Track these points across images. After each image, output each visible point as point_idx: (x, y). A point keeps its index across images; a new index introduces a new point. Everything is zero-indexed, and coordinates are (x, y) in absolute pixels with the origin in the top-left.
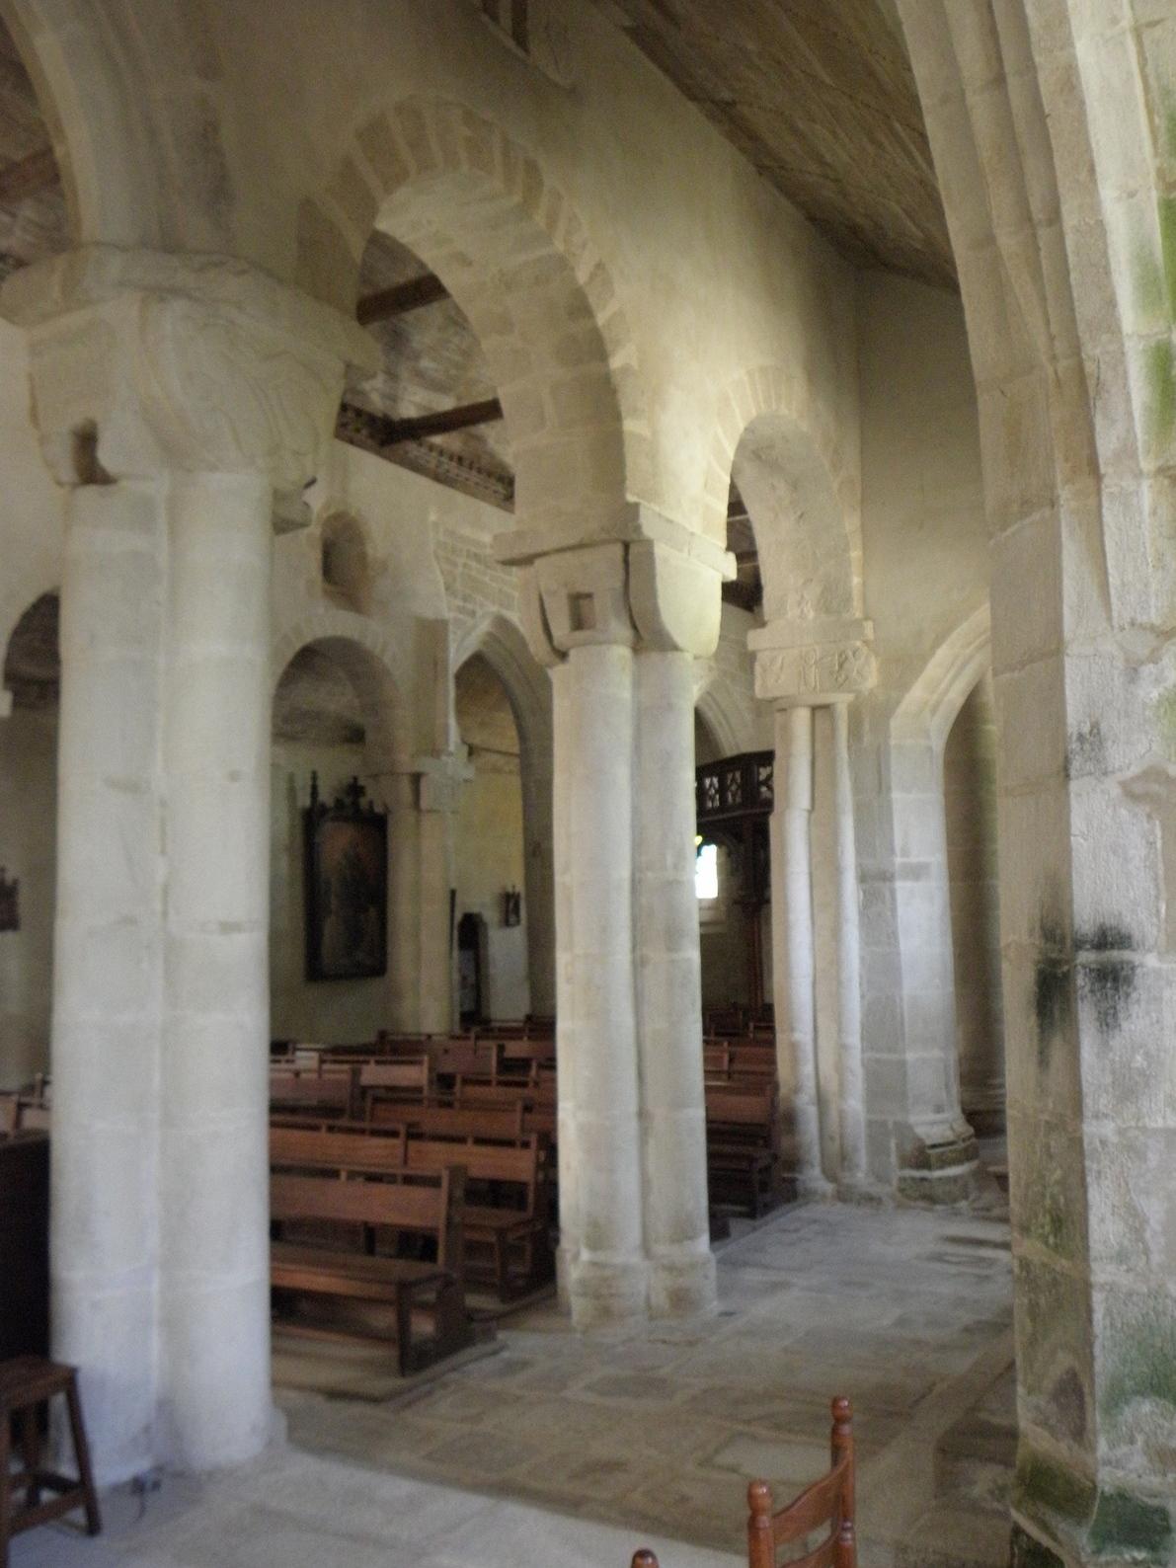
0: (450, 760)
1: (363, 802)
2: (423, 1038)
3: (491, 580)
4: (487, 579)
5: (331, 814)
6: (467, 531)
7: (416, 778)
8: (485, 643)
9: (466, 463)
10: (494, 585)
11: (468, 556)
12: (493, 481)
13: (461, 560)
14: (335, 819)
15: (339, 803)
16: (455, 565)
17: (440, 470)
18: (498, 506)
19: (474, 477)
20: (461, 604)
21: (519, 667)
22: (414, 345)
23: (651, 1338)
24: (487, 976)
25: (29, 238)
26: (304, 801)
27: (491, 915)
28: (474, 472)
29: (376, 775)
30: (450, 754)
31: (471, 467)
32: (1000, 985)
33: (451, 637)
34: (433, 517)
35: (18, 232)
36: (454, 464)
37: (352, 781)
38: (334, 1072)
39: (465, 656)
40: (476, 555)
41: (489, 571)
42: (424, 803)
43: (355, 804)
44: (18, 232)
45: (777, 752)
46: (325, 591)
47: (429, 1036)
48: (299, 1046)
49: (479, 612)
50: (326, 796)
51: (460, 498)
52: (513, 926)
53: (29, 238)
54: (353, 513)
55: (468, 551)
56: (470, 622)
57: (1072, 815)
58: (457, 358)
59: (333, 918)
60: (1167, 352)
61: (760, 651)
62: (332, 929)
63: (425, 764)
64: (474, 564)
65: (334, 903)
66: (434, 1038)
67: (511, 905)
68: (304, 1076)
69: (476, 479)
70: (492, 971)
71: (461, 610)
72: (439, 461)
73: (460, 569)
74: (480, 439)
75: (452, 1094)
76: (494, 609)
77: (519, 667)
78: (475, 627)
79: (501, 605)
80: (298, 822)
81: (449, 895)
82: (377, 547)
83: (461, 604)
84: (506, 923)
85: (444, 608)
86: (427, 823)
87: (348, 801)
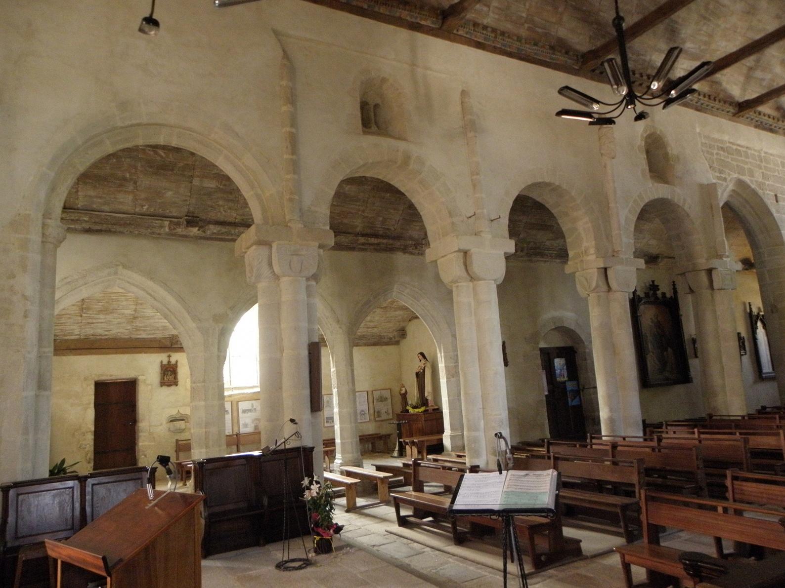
3: (732, 160)
4: (730, 160)
6: (716, 136)
7: (710, 272)
9: (712, 98)
10: (733, 162)
11: (718, 149)
12: (727, 105)
13: (715, 151)
14: (645, 303)
15: (647, 295)
16: (712, 154)
18: (730, 120)
19: (717, 105)
20: (719, 175)
21: (752, 207)
22: (683, 36)
23: (204, 398)
25: (497, 17)
28: (717, 102)
29: (684, 273)
31: (715, 100)
35: (491, 14)
36: (706, 99)
37: (651, 283)
38: (708, 439)
41: (730, 156)
42: (716, 285)
43: (655, 294)
44: (491, 14)
46: (651, 176)
48: (413, 397)
49: (729, 179)
53: (497, 17)
55: (718, 146)
56: (725, 184)
57: (129, 355)
58: (705, 39)
60: (402, 237)
63: (715, 263)
64: (722, 153)
65: (650, 346)
69: (717, 106)
71: (719, 178)
72: (698, 98)
73: (715, 156)
74: (718, 83)
75: (657, 436)
76: (736, 176)
77: (752, 207)
78: (727, 186)
79: (739, 173)
81: (305, 353)
82: (673, 149)
85: (710, 177)
86: (718, 296)
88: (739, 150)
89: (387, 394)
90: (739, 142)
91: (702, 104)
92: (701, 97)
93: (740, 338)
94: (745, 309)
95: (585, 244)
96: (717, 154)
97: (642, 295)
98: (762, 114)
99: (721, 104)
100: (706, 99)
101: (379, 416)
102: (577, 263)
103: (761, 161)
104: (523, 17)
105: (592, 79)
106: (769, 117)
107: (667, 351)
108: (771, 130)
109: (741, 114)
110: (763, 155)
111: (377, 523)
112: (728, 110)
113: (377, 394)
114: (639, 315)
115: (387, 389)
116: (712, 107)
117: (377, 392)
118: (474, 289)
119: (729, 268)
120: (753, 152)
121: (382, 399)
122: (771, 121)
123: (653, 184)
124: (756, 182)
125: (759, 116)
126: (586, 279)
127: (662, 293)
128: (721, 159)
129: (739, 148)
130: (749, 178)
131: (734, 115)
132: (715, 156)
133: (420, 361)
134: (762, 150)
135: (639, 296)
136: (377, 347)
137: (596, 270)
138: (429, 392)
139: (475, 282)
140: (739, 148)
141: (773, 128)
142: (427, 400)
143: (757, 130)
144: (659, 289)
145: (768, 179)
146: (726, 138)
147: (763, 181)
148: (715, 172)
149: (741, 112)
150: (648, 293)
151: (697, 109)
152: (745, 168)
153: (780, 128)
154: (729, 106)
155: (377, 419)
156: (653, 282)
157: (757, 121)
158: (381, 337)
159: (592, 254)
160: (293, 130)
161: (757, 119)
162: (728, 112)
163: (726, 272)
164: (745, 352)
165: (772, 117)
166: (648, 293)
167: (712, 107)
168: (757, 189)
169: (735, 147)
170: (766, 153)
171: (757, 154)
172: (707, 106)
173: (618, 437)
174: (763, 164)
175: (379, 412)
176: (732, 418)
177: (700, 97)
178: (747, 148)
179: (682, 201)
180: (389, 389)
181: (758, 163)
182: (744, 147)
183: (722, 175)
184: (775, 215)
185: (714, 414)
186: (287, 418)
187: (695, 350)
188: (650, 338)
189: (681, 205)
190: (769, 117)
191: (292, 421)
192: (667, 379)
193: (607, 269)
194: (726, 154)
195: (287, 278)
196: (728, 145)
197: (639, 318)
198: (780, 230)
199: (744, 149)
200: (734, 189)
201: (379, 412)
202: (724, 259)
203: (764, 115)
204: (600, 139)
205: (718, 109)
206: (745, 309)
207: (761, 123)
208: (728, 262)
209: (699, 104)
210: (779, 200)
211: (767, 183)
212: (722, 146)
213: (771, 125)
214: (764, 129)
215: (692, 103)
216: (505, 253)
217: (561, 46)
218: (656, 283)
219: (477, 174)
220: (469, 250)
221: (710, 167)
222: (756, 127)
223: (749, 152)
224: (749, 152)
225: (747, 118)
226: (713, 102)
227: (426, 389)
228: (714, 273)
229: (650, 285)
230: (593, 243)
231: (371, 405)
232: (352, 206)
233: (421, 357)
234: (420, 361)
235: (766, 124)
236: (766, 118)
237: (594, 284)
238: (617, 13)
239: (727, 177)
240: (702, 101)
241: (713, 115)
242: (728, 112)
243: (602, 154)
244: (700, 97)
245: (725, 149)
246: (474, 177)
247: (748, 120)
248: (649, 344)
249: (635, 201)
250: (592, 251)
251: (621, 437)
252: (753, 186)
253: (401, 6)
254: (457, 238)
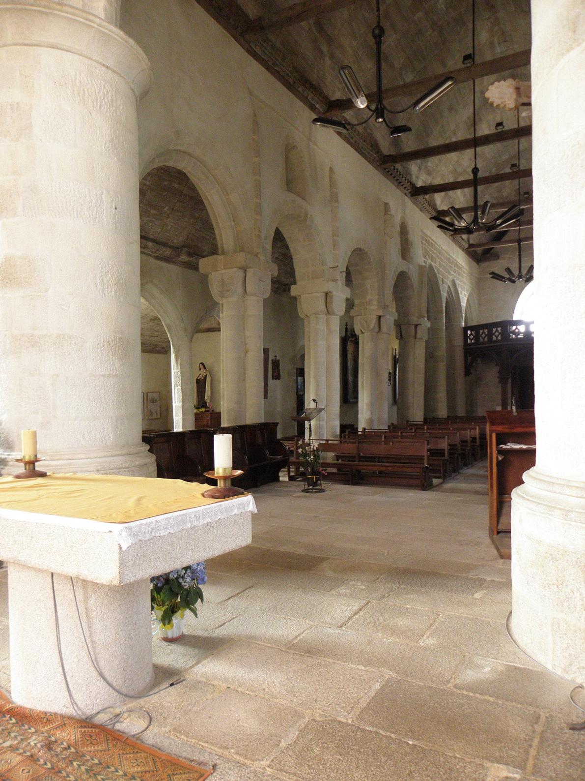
36: (427, 204)
89: (156, 396)
93: (390, 373)
94: (393, 354)
95: (369, 297)
100: (427, 204)
101: (151, 415)
102: (361, 310)
104: (364, 118)
105: (383, 174)
113: (150, 395)
117: (150, 394)
118: (327, 320)
121: (153, 401)
126: (366, 322)
133: (200, 369)
136: (151, 355)
137: (375, 316)
138: (208, 396)
139: (329, 316)
142: (206, 402)
155: (150, 418)
158: (156, 346)
159: (375, 305)
160: (258, 178)
175: (151, 412)
176: (415, 423)
186: (311, 399)
187: (390, 377)
191: (314, 400)
195: (254, 298)
201: (151, 412)
204: (385, 221)
206: (393, 354)
216: (346, 298)
217: (375, 146)
219: (338, 236)
220: (330, 292)
227: (206, 393)
228: (418, 328)
230: (377, 297)
231: (145, 406)
232: (209, 233)
233: (202, 367)
234: (200, 369)
237: (372, 326)
238: (476, 165)
243: (385, 234)
246: (335, 238)
250: (375, 303)
253: (311, 89)
254: (328, 282)
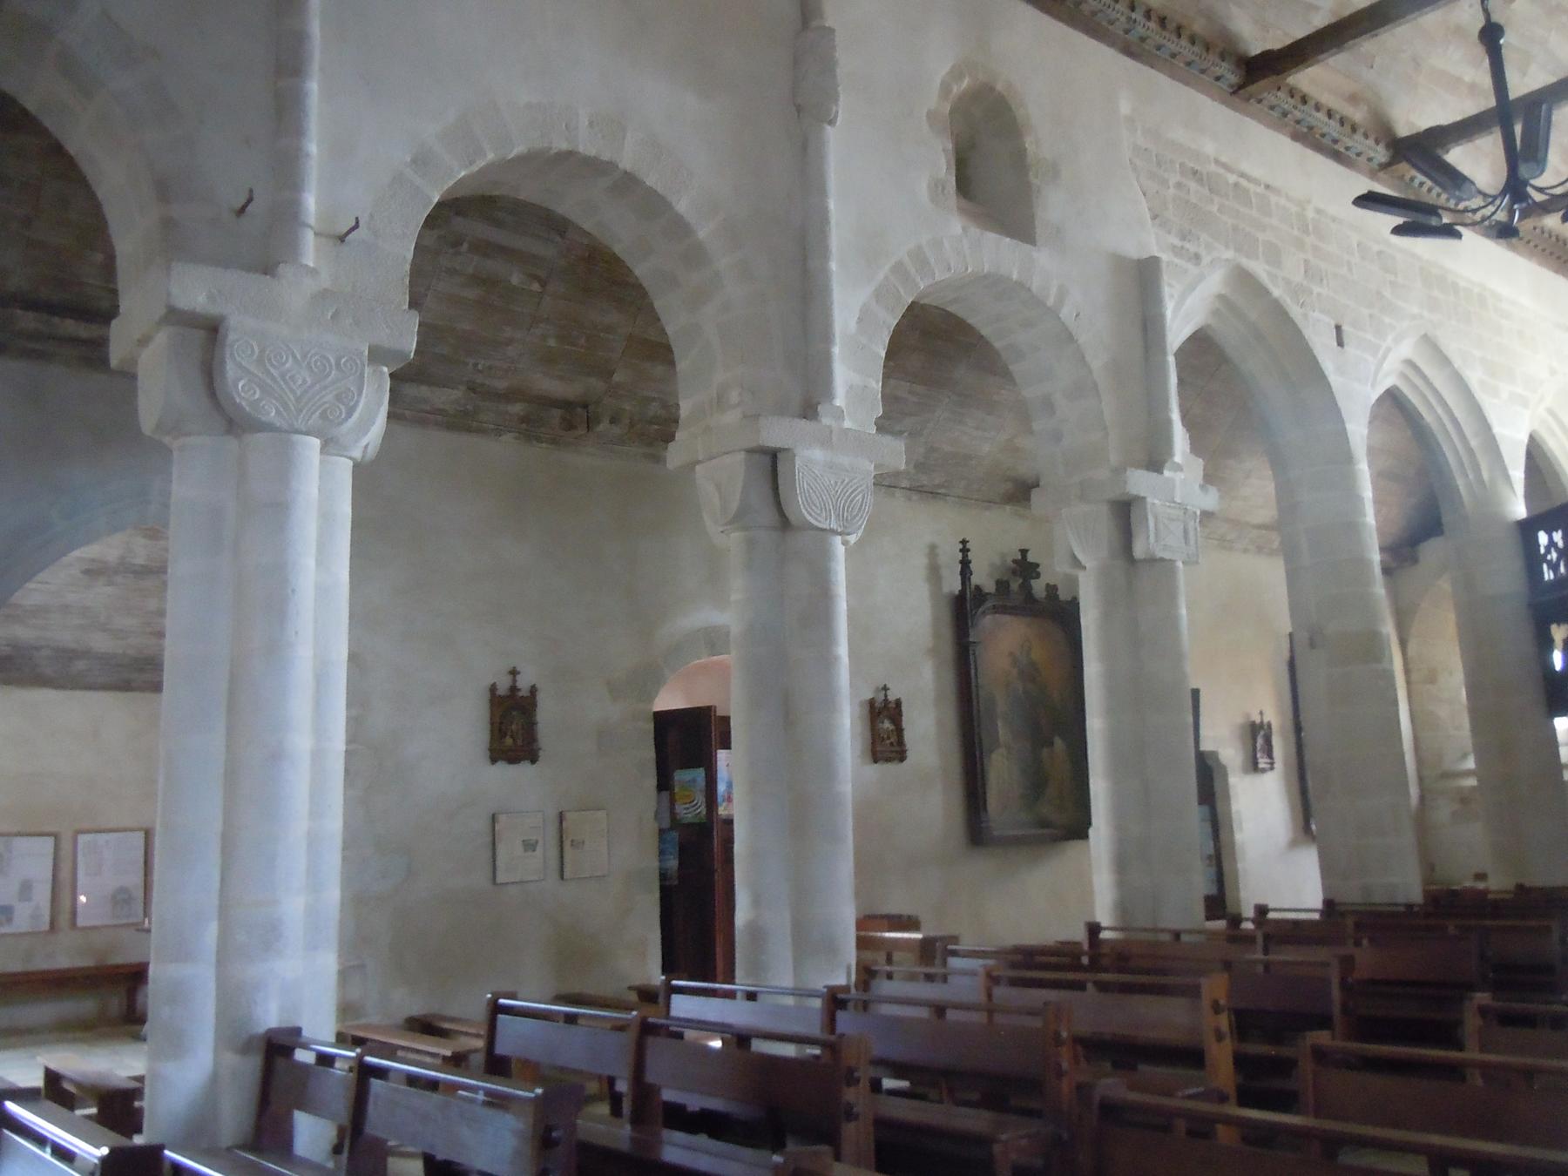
0: (1179, 477)
1: (1038, 587)
2: (1166, 937)
5: (989, 604)
6: (1178, 134)
8: (1216, 313)
11: (1183, 173)
12: (1213, 57)
14: (997, 610)
15: (1002, 586)
16: (1164, 183)
17: (1130, 37)
18: (1224, 102)
20: (1177, 242)
24: (1232, 843)
26: (953, 584)
27: (1230, 754)
28: (1184, 42)
30: (1179, 468)
32: (152, 889)
33: (1166, 290)
34: (1125, 108)
36: (1152, 25)
39: (1187, 332)
40: (1195, 173)
43: (1026, 588)
45: (1196, 804)
47: (1177, 935)
50: (982, 577)
51: (1160, 80)
52: (1264, 771)
54: (999, 87)
59: (1002, 751)
61: (949, 974)
62: (1002, 771)
63: (1139, 482)
64: (1193, 185)
65: (1003, 732)
66: (1185, 938)
67: (1260, 741)
68: (951, 1015)
70: (1239, 837)
71: (1177, 251)
79: (1238, 250)
80: (946, 616)
83: (1177, 242)
84: (1253, 767)
87: (1015, 585)
88: (1246, 191)
90: (1245, 166)
91: (1143, 39)
92: (1138, 15)
96: (1179, 185)
97: (989, 587)
98: (1312, 103)
99: (1196, 49)
103: (1306, 231)
106: (1330, 114)
107: (1052, 744)
108: (1337, 156)
109: (1252, 88)
110: (1310, 214)
111: (459, 1164)
112: (1219, 71)
114: (971, 639)
115: (132, 830)
116: (1173, 56)
119: (1179, 501)
120: (1283, 201)
122: (1333, 128)
123: (964, 229)
124: (1288, 282)
125: (1302, 108)
127: (1048, 585)
128: (1187, 202)
129: (1244, 182)
130: (1267, 267)
131: (1237, 90)
132: (1172, 191)
134: (1309, 202)
135: (978, 588)
137: (741, 456)
140: (1244, 182)
141: (1342, 150)
143: (1298, 146)
144: (1038, 576)
145: (1322, 280)
146: (1209, 148)
147: (1305, 283)
148: (1169, 233)
149: (1253, 83)
150: (1007, 583)
151: (1128, 51)
152: (1258, 240)
153: (1358, 155)
154: (1218, 60)
156: (1024, 552)
157: (1298, 122)
161: (1298, 115)
162: (1218, 79)
163: (1169, 510)
164: (1272, 764)
165: (1338, 117)
166: (1007, 583)
167: (1173, 56)
168: (1288, 300)
169: (1232, 178)
170: (1319, 211)
171: (1294, 209)
172: (1159, 48)
173: (1163, 930)
174: (1310, 240)
177: (1134, 16)
178: (1267, 187)
179: (1054, 291)
180: (139, 829)
181: (1296, 232)
182: (1260, 185)
183: (1187, 245)
184: (1334, 379)
185: (1271, 906)
188: (1002, 706)
189: (1050, 302)
190: (1330, 114)
192: (1044, 823)
193: (779, 455)
194: (1206, 191)
196: (1213, 167)
197: (971, 648)
198: (1343, 422)
199: (1260, 190)
200: (1223, 292)
202: (1167, 473)
203: (1318, 107)
205: (1189, 64)
207: (1311, 128)
208: (1178, 483)
209: (1130, 37)
210: (1346, 340)
211: (1316, 289)
212: (1197, 167)
213: (1335, 141)
214: (1319, 148)
215: (1110, 27)
218: (1031, 558)
221: (1154, 217)
222: (1296, 137)
223: (1273, 199)
224: (1273, 199)
225: (1272, 108)
226: (1174, 38)
229: (1015, 561)
235: (1323, 135)
236: (1321, 116)
239: (1203, 252)
240: (1140, 30)
241: (1173, 76)
242: (1218, 79)
244: (1134, 16)
245: (1205, 178)
247: (1275, 114)
248: (1000, 724)
249: (899, 268)
251: (1169, 931)
252: (1276, 292)
